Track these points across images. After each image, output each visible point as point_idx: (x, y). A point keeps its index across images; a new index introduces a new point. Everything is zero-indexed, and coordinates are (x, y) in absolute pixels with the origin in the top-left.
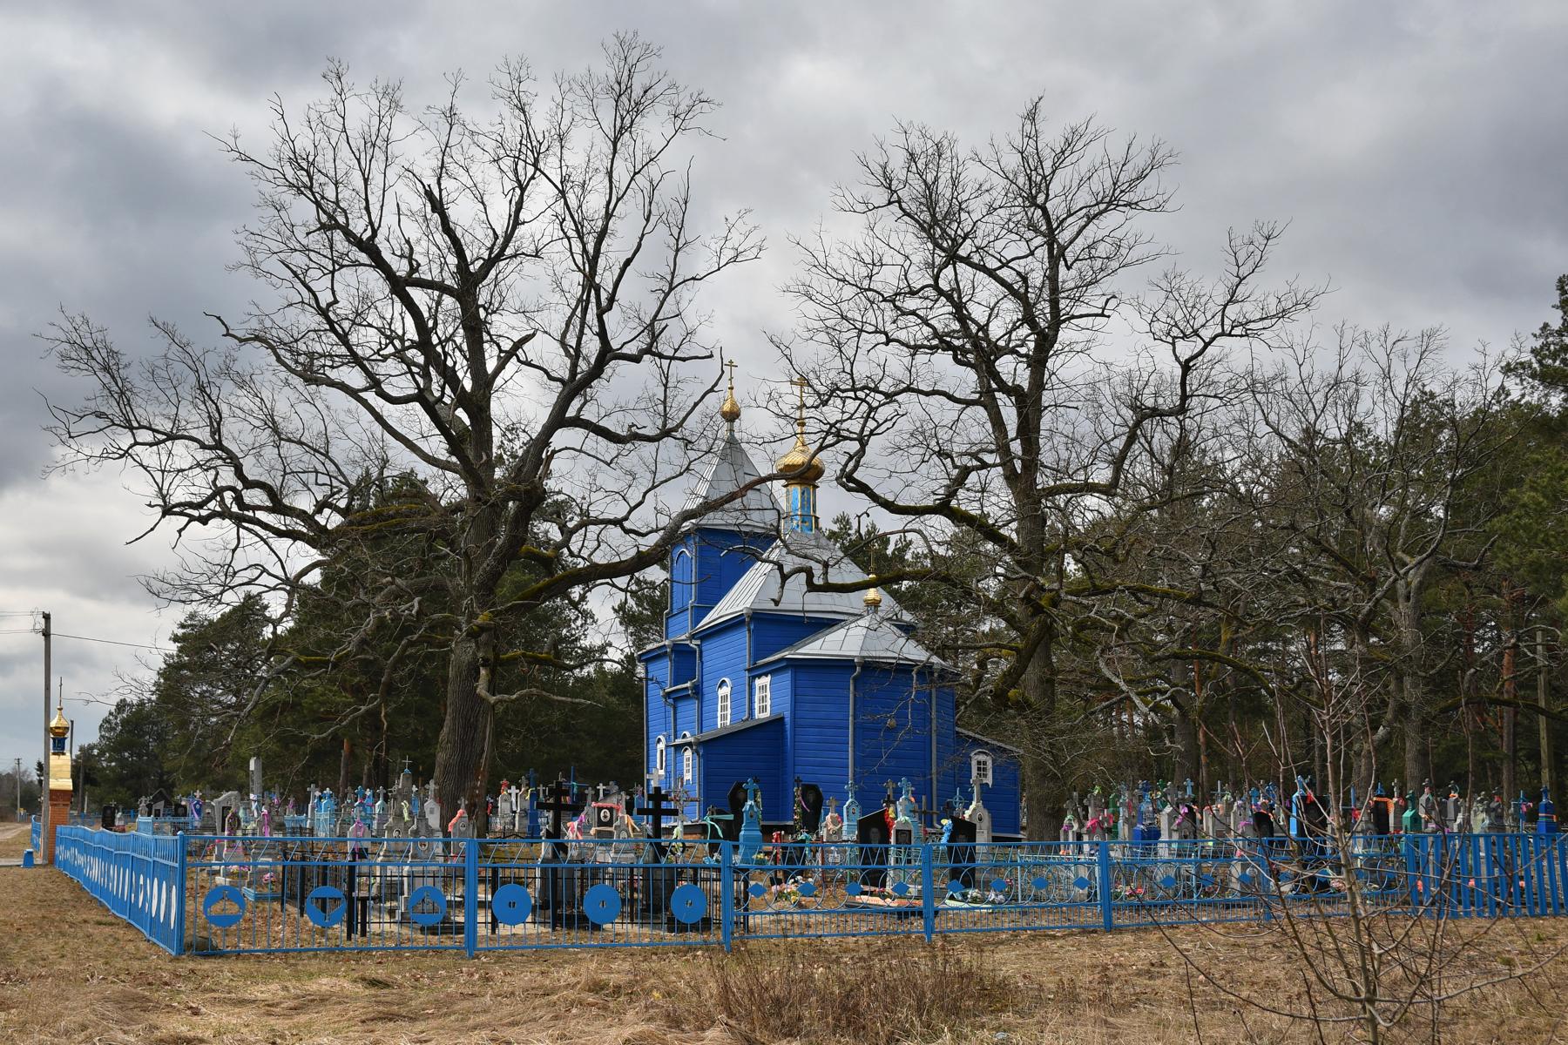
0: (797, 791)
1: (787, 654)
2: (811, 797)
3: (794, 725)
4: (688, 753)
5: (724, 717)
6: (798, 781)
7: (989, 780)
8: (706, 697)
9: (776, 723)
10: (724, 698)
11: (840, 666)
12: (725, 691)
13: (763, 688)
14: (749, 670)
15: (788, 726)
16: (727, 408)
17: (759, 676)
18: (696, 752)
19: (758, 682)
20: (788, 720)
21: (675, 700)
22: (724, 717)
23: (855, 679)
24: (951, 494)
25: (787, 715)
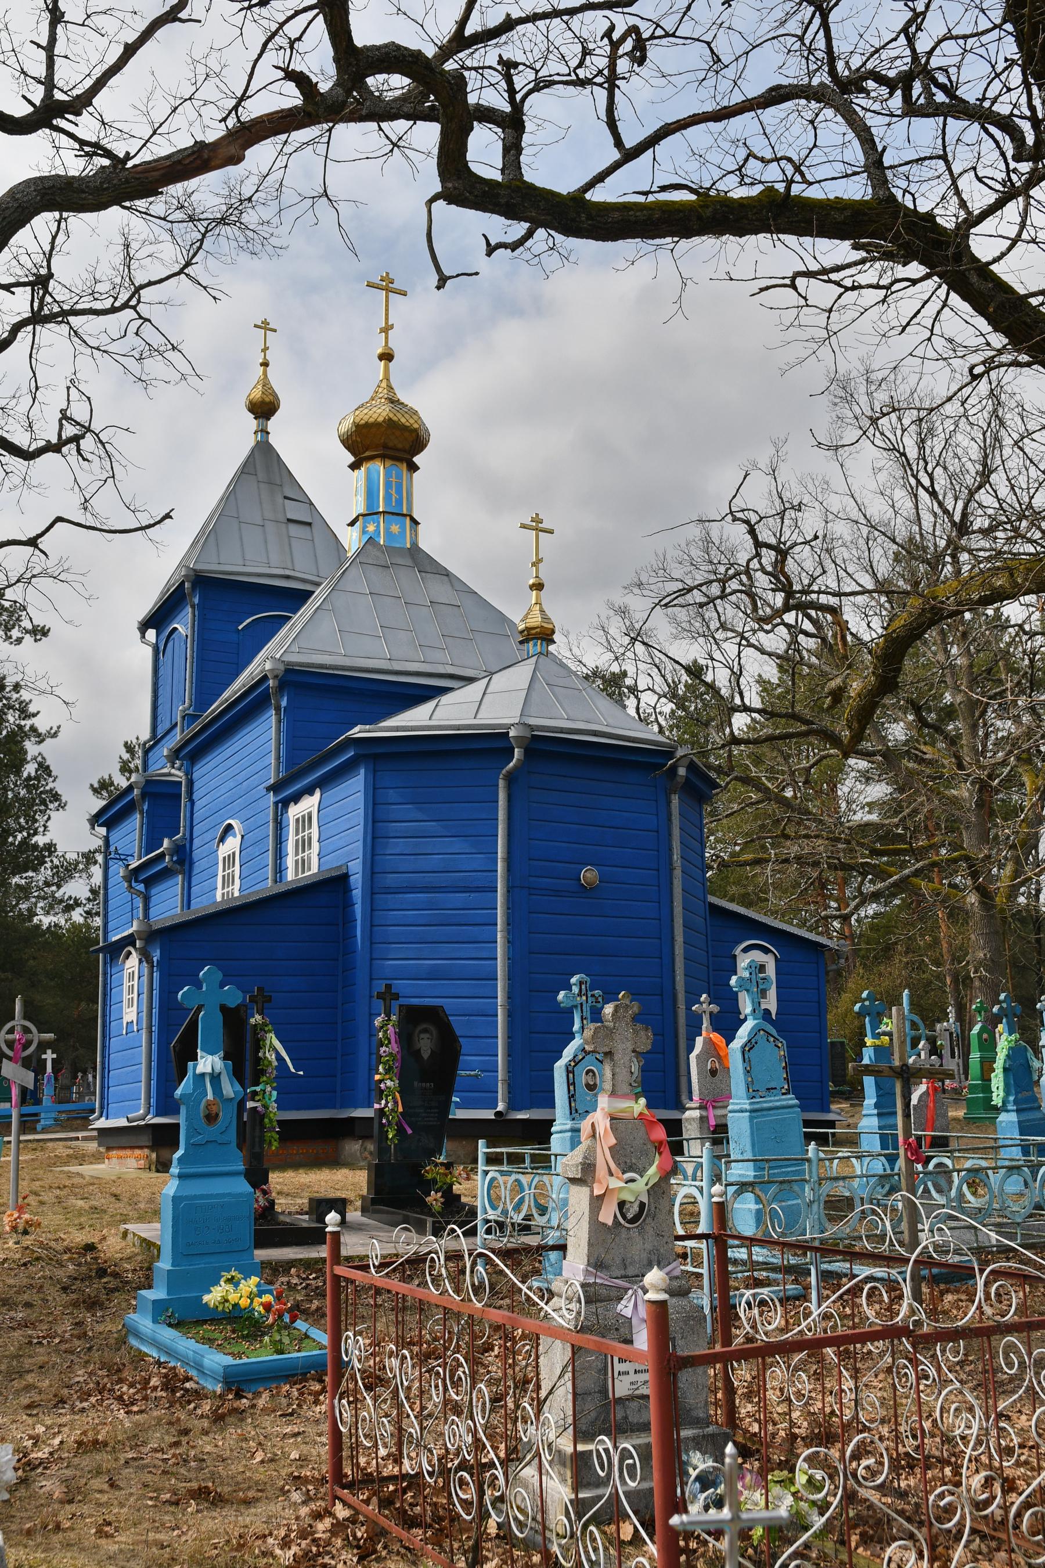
0: (385, 1025)
1: (358, 732)
2: (426, 1044)
3: (372, 890)
4: (132, 963)
5: (228, 881)
6: (389, 995)
7: (771, 1003)
8: (198, 867)
9: (334, 884)
10: (229, 860)
11: (482, 747)
12: (232, 844)
13: (305, 821)
14: (275, 788)
15: (357, 894)
16: (257, 394)
17: (296, 798)
18: (145, 956)
19: (295, 811)
20: (357, 880)
21: (149, 882)
22: (228, 881)
23: (511, 779)
24: (756, 157)
25: (356, 870)
